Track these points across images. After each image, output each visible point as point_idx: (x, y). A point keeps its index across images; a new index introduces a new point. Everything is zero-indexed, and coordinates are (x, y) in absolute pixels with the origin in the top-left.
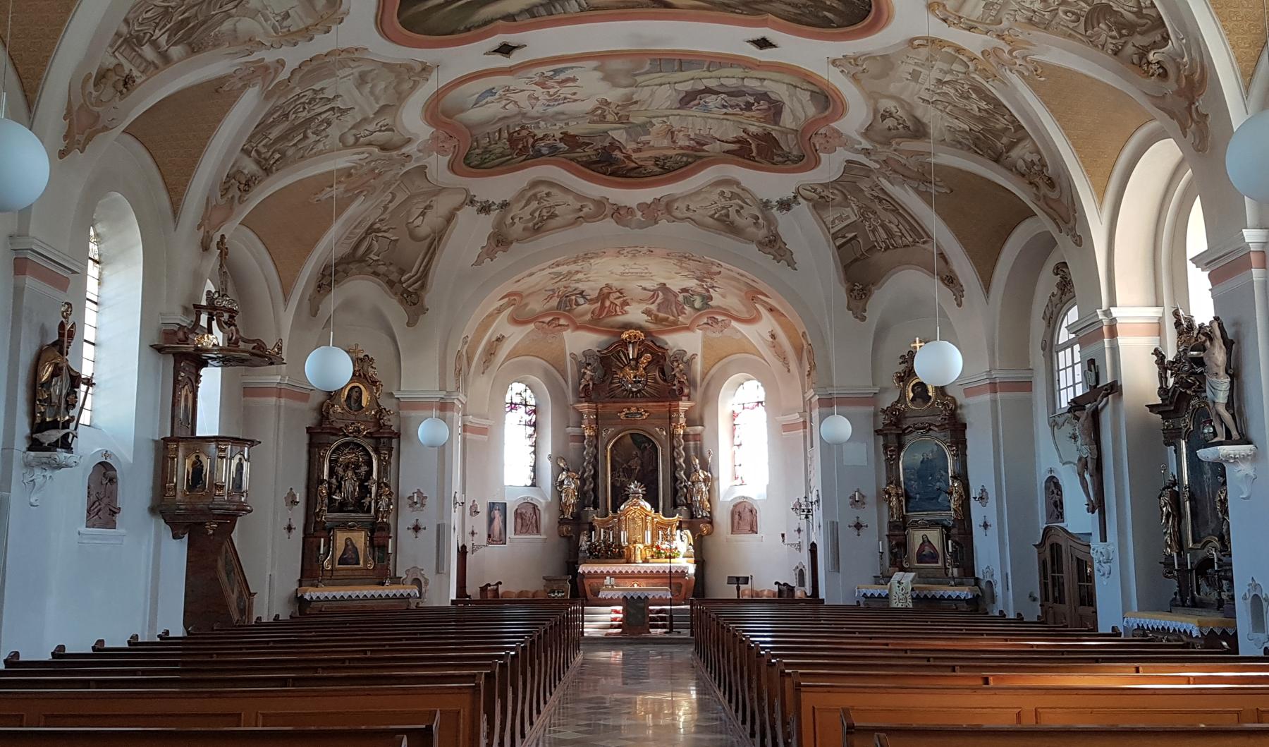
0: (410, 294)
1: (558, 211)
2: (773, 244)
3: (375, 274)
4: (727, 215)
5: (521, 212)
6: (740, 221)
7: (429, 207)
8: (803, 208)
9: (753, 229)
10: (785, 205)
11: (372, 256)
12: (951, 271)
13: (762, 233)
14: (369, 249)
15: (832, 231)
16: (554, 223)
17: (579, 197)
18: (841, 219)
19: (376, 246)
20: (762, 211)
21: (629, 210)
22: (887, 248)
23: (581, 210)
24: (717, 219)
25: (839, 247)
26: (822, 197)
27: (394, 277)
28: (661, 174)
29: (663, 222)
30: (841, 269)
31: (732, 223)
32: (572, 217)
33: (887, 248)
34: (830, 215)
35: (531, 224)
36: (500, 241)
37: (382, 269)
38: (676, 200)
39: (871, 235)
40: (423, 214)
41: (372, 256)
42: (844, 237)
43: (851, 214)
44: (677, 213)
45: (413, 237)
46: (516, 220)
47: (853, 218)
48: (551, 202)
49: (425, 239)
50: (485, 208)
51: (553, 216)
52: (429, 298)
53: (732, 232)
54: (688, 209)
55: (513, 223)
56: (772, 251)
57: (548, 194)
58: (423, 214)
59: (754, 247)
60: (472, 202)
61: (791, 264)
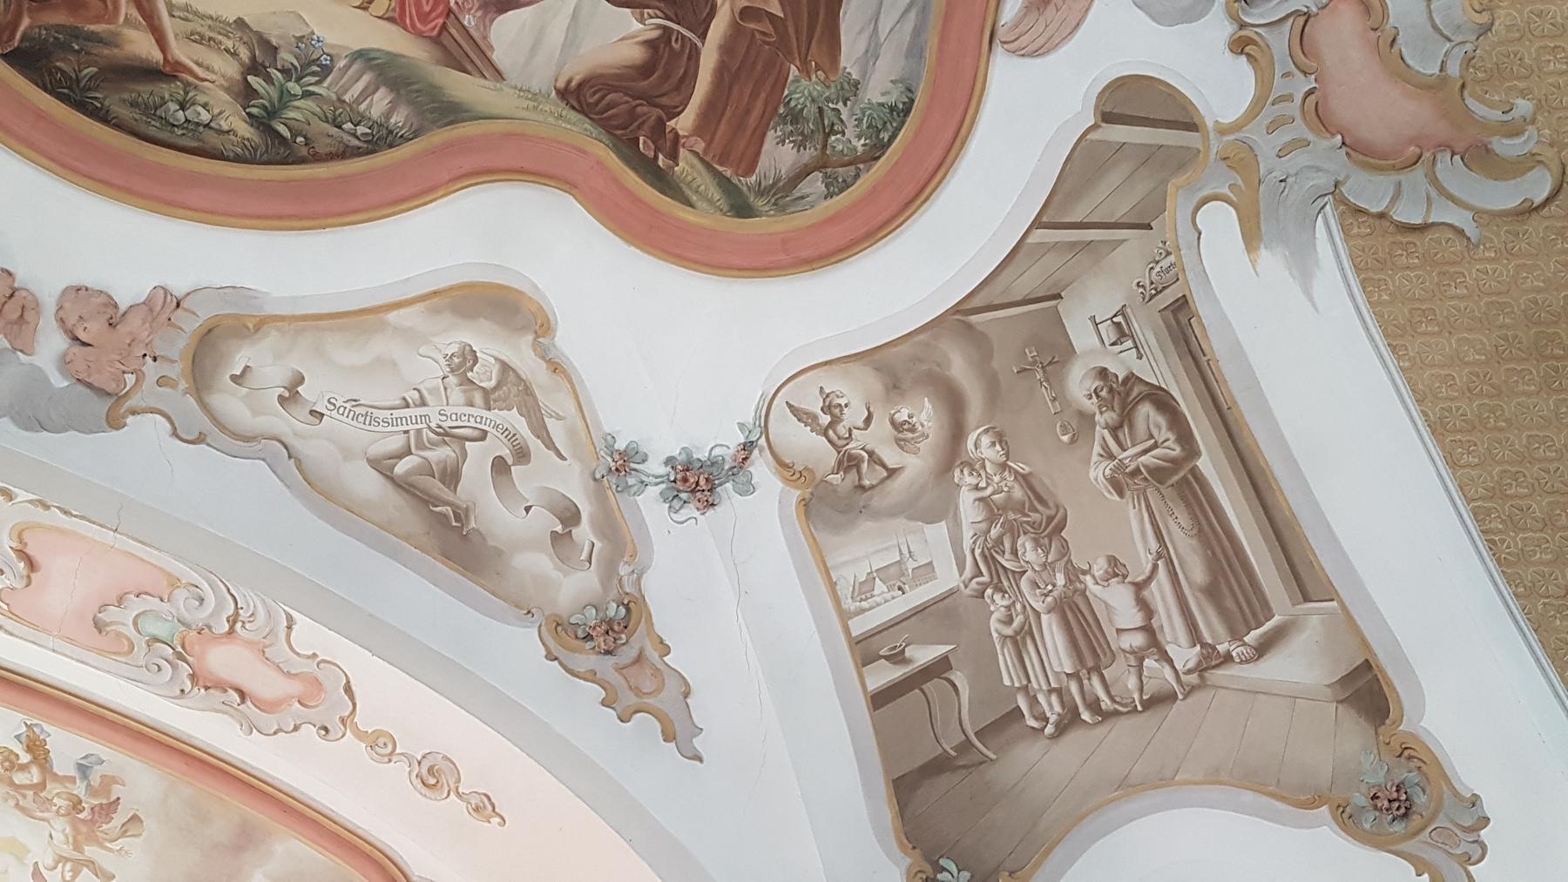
2: (610, 639)
4: (451, 476)
6: (497, 516)
8: (762, 509)
9: (540, 562)
10: (696, 482)
12: (1410, 752)
13: (574, 587)
15: (859, 627)
18: (897, 576)
20: (600, 497)
22: (1069, 721)
24: (402, 485)
25: (879, 700)
26: (849, 463)
28: (246, 157)
29: (147, 430)
30: (882, 788)
31: (462, 515)
33: (1069, 721)
34: (862, 552)
38: (262, 324)
39: (1005, 658)
42: (898, 658)
43: (939, 557)
44: (231, 403)
47: (948, 578)
53: (447, 556)
54: (290, 397)
56: (606, 665)
59: (526, 642)
61: (677, 732)
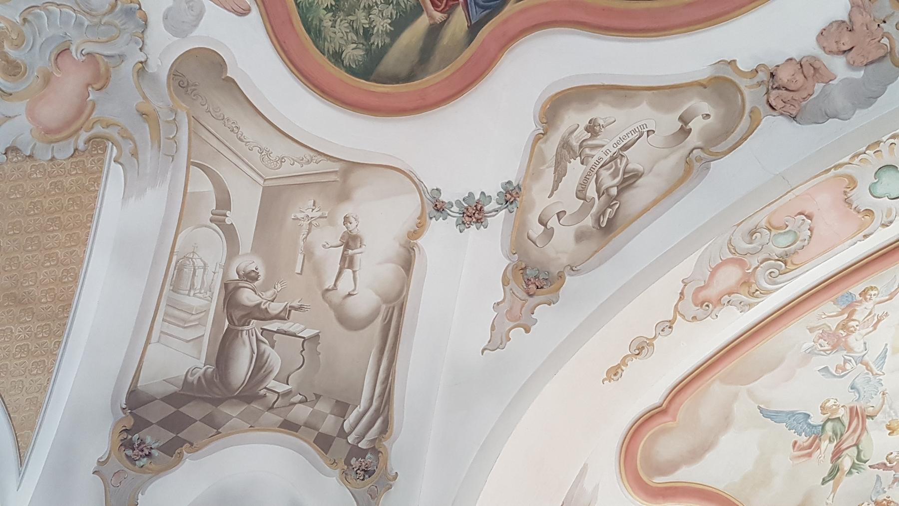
0: (362, 453)
1: (635, 159)
3: (289, 426)
5: (558, 198)
7: (350, 241)
11: (271, 383)
14: (260, 365)
16: (639, 196)
17: (666, 93)
19: (275, 359)
21: (809, 68)
23: (685, 132)
27: (329, 425)
32: (672, 161)
35: (589, 221)
36: (534, 280)
37: (301, 413)
40: (347, 262)
41: (271, 383)
45: (346, 321)
46: (553, 223)
48: (609, 143)
49: (369, 320)
50: (473, 213)
51: (630, 180)
52: (397, 449)
55: (549, 233)
57: (592, 129)
58: (347, 262)
60: (440, 209)
